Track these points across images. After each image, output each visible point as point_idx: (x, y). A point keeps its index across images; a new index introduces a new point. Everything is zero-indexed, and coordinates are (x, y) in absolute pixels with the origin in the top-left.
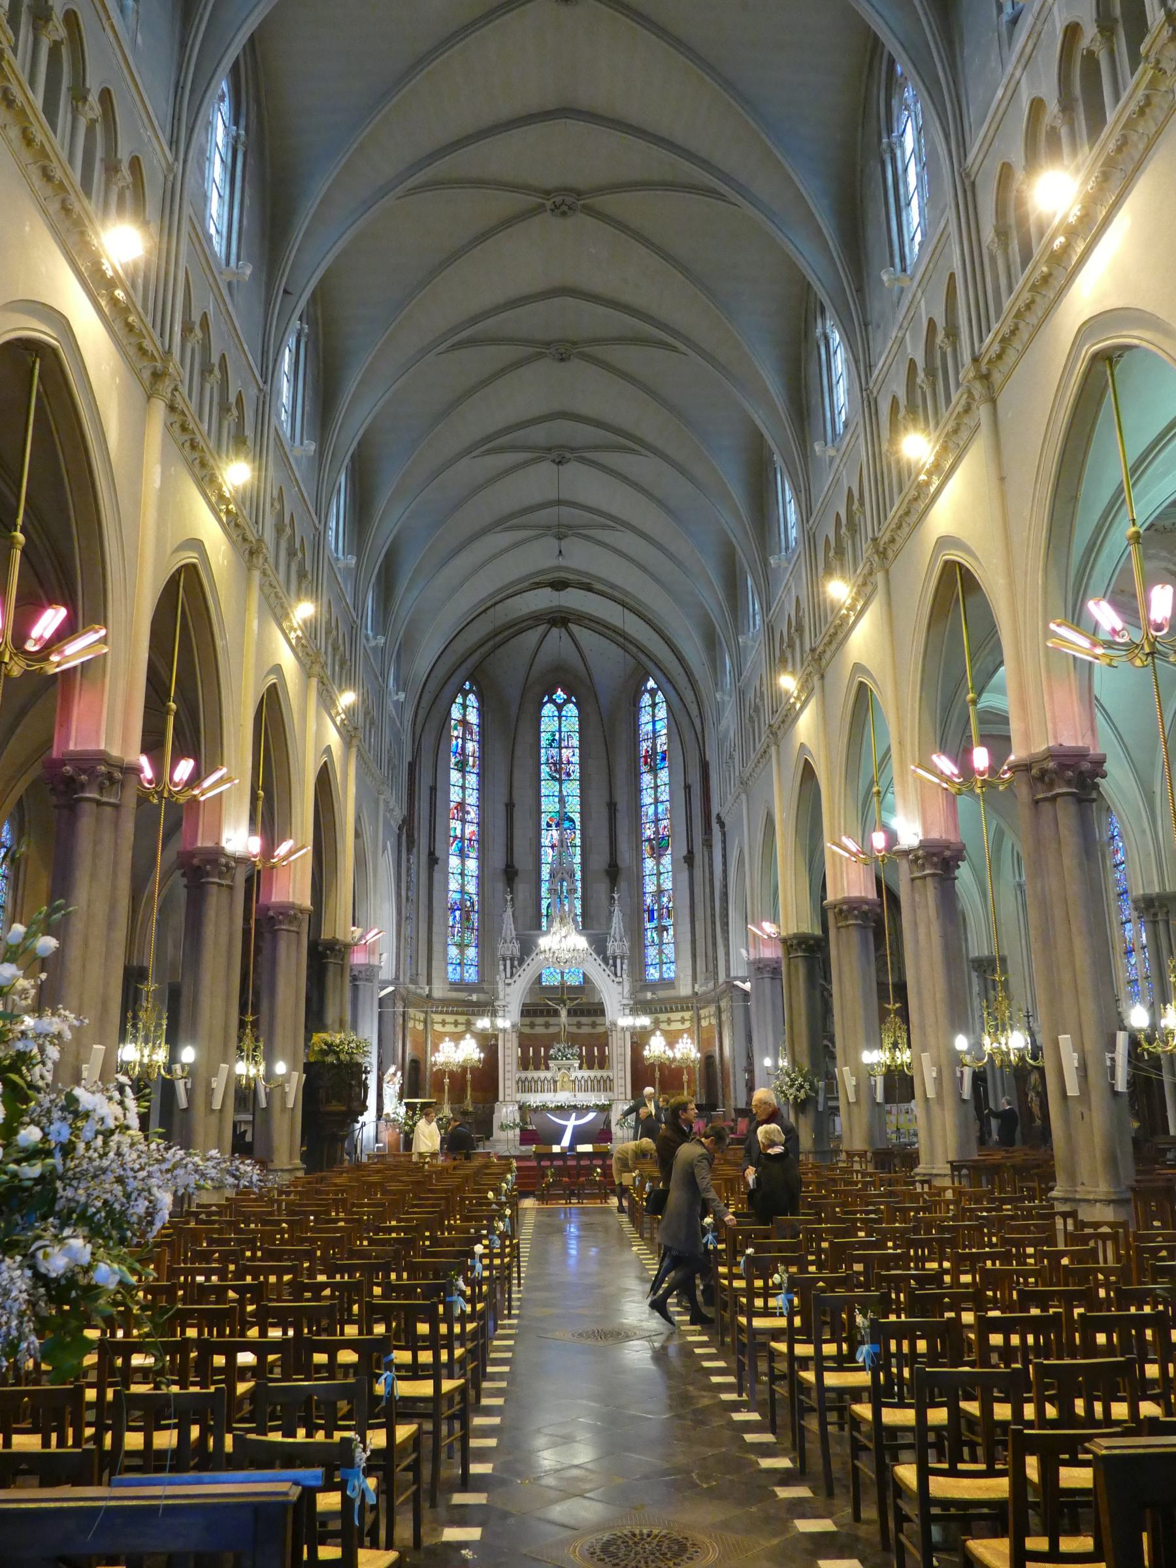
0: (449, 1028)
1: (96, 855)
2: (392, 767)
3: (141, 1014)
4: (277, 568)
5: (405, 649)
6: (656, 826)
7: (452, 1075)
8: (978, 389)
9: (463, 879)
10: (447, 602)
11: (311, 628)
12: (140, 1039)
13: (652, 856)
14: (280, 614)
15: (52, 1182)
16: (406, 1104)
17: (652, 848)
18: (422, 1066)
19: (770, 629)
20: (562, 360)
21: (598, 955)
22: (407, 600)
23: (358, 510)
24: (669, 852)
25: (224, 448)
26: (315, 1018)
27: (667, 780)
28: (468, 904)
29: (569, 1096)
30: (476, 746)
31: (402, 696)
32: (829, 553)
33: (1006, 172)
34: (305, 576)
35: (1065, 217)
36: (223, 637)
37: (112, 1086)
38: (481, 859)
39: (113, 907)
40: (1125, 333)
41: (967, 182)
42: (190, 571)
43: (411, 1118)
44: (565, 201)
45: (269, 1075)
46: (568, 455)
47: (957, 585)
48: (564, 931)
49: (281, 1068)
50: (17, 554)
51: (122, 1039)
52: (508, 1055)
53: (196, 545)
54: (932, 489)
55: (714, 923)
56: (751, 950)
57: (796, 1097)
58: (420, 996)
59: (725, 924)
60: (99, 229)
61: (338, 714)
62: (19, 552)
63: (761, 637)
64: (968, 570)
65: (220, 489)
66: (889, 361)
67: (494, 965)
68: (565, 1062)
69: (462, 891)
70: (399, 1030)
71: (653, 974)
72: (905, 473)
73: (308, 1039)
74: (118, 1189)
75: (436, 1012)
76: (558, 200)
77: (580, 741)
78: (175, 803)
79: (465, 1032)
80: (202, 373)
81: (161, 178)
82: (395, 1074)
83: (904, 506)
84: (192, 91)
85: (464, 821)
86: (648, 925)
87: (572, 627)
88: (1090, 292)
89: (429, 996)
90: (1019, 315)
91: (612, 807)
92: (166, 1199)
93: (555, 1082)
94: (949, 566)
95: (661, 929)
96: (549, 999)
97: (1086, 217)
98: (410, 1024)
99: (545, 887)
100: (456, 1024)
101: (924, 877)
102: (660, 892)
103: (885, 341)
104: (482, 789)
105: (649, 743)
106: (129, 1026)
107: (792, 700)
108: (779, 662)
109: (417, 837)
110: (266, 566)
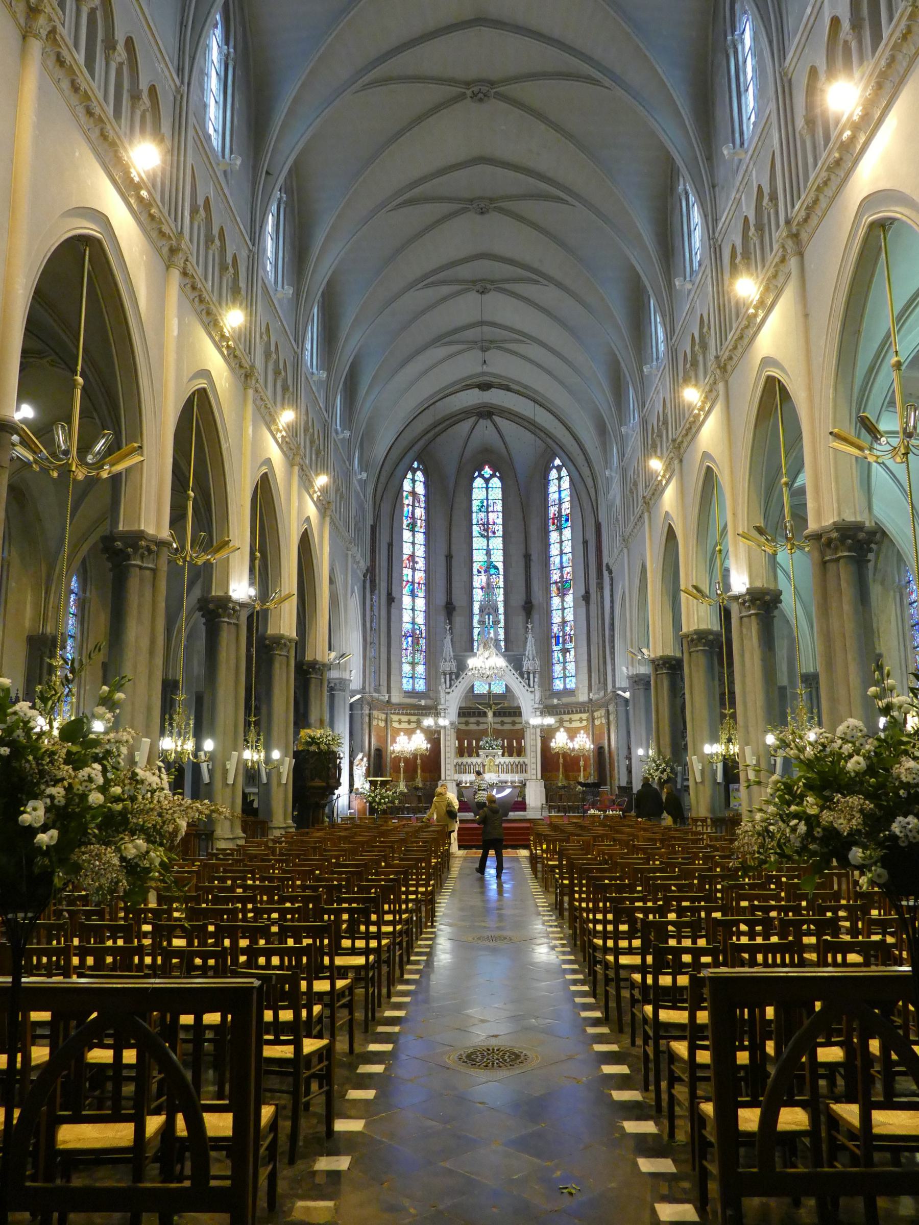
0: (404, 725)
1: (140, 606)
2: (358, 529)
3: (174, 716)
4: (266, 387)
5: (366, 440)
6: (562, 572)
7: (406, 760)
8: (790, 244)
9: (413, 613)
10: (394, 405)
11: (292, 430)
12: (175, 734)
13: (558, 595)
14: (269, 420)
15: (126, 815)
16: (370, 781)
17: (558, 589)
18: (384, 754)
19: (644, 422)
20: (482, 213)
21: (516, 671)
22: (366, 404)
23: (325, 344)
24: (571, 591)
25: (224, 299)
26: (301, 719)
27: (569, 537)
28: (418, 632)
29: (494, 774)
30: (423, 511)
31: (364, 475)
32: (686, 366)
33: (813, 72)
34: (288, 389)
35: (851, 115)
36: (227, 440)
37: (155, 768)
38: (428, 597)
39: (153, 642)
40: (892, 208)
41: (785, 79)
42: (202, 393)
43: (374, 792)
44: (481, 90)
45: (268, 760)
46: (489, 286)
47: (775, 394)
48: (487, 654)
49: (276, 755)
50: (78, 392)
51: (162, 733)
52: (448, 746)
53: (206, 374)
54: (758, 320)
55: (604, 647)
56: (630, 668)
57: (660, 778)
58: (383, 702)
59: (613, 647)
60: (127, 146)
61: (315, 492)
62: (79, 391)
63: (638, 430)
64: (783, 385)
65: (222, 331)
66: (730, 217)
67: (437, 678)
68: (491, 751)
69: (413, 623)
70: (366, 727)
71: (558, 685)
72: (739, 307)
73: (296, 733)
74: (159, 820)
75: (394, 714)
76: (476, 89)
77: (503, 506)
78: (195, 565)
79: (416, 728)
80: (206, 242)
81: (172, 98)
82: (362, 760)
83: (739, 332)
84: (193, 28)
85: (414, 569)
86: (555, 648)
87: (496, 418)
88: (870, 173)
89: (389, 702)
90: (819, 189)
91: (527, 557)
92: (183, 824)
93: (484, 766)
94: (771, 380)
95: (565, 651)
96: (479, 704)
97: (866, 116)
98: (375, 723)
99: (476, 619)
100: (409, 722)
101: (750, 616)
102: (564, 623)
103: (728, 199)
104: (427, 544)
105: (556, 508)
106: (167, 724)
107: (659, 478)
108: (651, 448)
109: (378, 581)
110: (258, 385)
